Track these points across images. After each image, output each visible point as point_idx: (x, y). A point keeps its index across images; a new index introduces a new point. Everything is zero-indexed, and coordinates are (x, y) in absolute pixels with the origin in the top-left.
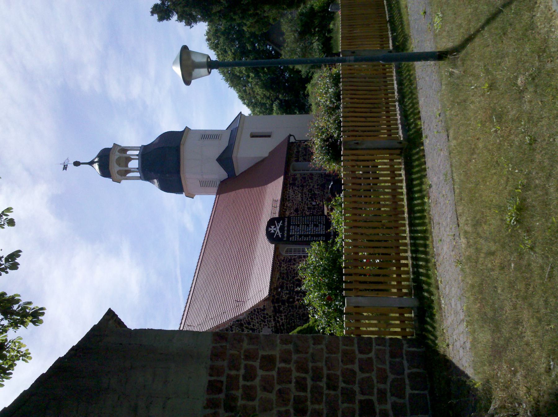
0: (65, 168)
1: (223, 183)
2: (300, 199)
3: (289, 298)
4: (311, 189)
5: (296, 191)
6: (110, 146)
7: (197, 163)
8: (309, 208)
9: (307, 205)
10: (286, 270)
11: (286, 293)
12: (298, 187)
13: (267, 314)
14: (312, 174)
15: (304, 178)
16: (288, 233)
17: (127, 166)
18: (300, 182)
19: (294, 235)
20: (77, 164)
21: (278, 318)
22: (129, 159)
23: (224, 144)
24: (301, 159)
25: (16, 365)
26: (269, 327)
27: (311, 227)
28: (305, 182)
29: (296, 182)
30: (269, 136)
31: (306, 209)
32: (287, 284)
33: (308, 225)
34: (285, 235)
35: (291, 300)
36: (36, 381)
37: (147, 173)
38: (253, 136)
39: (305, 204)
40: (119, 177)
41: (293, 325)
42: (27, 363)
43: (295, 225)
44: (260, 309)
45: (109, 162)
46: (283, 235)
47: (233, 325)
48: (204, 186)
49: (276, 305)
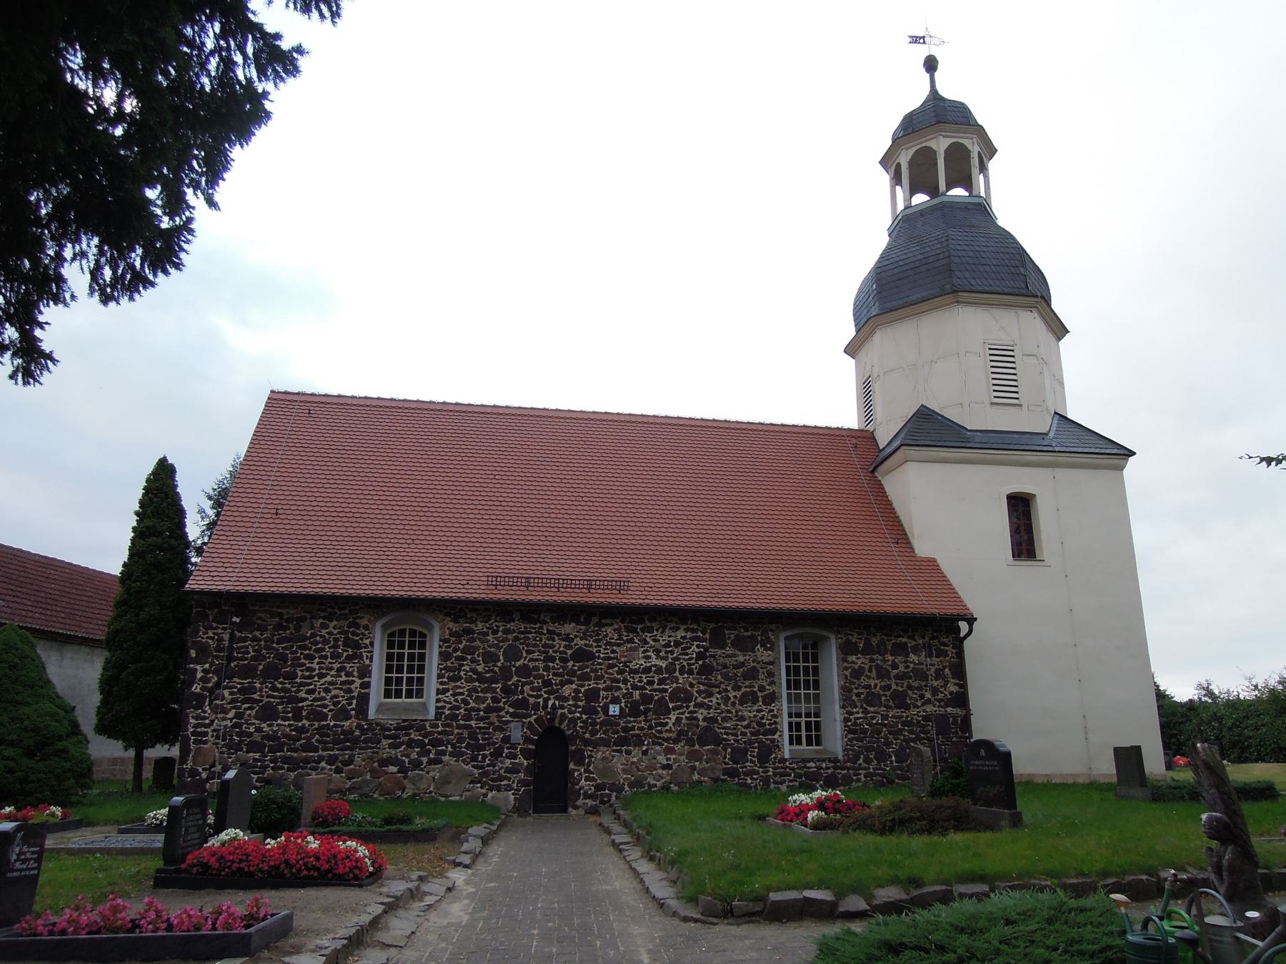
0: (916, 40)
5: (677, 652)
7: (951, 355)
11: (221, 640)
20: (931, 65)
32: (254, 639)
36: (94, 571)
42: (214, 212)
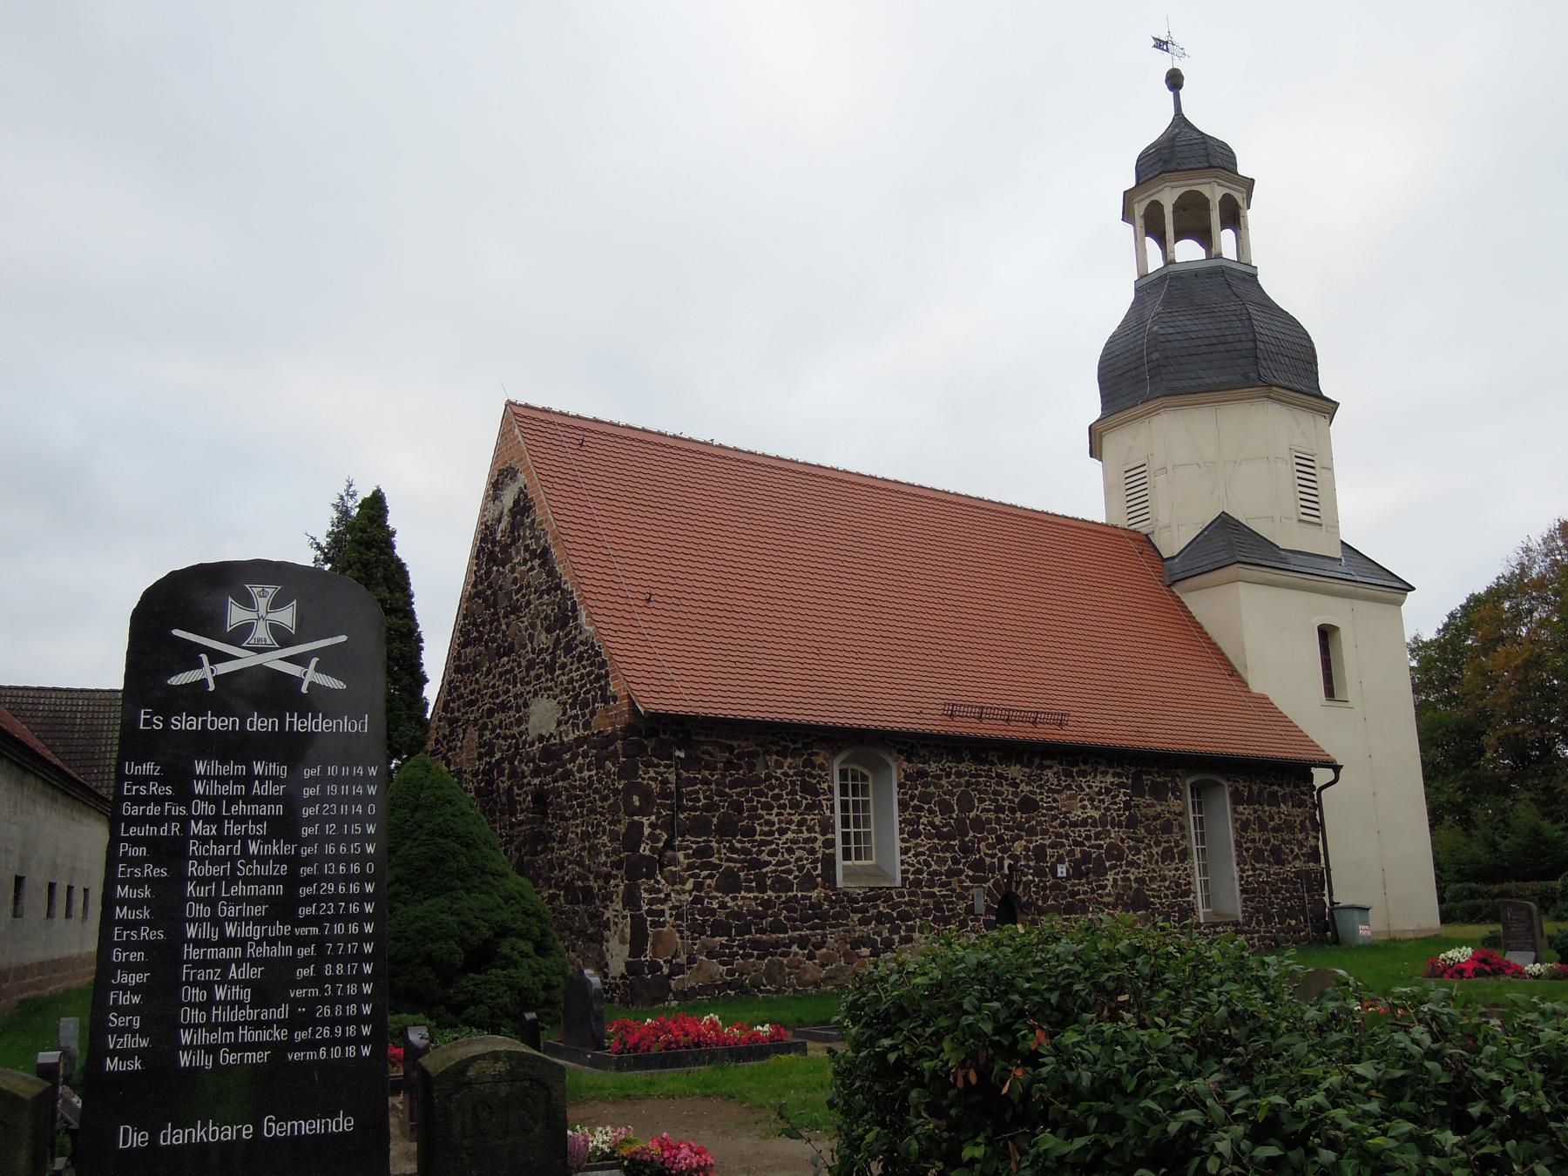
0: (1161, 44)
2: (1077, 814)
3: (646, 794)
5: (1108, 799)
6: (1243, 170)
7: (1210, 460)
8: (1040, 853)
9: (1052, 846)
10: (769, 777)
11: (665, 782)
12: (1127, 805)
13: (593, 713)
14: (1185, 855)
15: (1167, 829)
16: (208, 745)
17: (1179, 237)
18: (1150, 812)
19: (184, 796)
20: (1175, 81)
21: (585, 755)
22: (1205, 238)
23: (1289, 536)
24: (1246, 811)
26: (559, 724)
27: (263, 942)
28: (1149, 831)
29: (1148, 799)
30: (1330, 692)
31: (1038, 840)
32: (706, 782)
33: (282, 909)
34: (185, 723)
37: (1160, 293)
38: (1326, 634)
39: (1058, 835)
40: (1139, 210)
41: (568, 813)
43: (291, 802)
44: (608, 684)
45: (1187, 180)
46: (196, 698)
47: (563, 591)
48: (1133, 484)
49: (619, 744)
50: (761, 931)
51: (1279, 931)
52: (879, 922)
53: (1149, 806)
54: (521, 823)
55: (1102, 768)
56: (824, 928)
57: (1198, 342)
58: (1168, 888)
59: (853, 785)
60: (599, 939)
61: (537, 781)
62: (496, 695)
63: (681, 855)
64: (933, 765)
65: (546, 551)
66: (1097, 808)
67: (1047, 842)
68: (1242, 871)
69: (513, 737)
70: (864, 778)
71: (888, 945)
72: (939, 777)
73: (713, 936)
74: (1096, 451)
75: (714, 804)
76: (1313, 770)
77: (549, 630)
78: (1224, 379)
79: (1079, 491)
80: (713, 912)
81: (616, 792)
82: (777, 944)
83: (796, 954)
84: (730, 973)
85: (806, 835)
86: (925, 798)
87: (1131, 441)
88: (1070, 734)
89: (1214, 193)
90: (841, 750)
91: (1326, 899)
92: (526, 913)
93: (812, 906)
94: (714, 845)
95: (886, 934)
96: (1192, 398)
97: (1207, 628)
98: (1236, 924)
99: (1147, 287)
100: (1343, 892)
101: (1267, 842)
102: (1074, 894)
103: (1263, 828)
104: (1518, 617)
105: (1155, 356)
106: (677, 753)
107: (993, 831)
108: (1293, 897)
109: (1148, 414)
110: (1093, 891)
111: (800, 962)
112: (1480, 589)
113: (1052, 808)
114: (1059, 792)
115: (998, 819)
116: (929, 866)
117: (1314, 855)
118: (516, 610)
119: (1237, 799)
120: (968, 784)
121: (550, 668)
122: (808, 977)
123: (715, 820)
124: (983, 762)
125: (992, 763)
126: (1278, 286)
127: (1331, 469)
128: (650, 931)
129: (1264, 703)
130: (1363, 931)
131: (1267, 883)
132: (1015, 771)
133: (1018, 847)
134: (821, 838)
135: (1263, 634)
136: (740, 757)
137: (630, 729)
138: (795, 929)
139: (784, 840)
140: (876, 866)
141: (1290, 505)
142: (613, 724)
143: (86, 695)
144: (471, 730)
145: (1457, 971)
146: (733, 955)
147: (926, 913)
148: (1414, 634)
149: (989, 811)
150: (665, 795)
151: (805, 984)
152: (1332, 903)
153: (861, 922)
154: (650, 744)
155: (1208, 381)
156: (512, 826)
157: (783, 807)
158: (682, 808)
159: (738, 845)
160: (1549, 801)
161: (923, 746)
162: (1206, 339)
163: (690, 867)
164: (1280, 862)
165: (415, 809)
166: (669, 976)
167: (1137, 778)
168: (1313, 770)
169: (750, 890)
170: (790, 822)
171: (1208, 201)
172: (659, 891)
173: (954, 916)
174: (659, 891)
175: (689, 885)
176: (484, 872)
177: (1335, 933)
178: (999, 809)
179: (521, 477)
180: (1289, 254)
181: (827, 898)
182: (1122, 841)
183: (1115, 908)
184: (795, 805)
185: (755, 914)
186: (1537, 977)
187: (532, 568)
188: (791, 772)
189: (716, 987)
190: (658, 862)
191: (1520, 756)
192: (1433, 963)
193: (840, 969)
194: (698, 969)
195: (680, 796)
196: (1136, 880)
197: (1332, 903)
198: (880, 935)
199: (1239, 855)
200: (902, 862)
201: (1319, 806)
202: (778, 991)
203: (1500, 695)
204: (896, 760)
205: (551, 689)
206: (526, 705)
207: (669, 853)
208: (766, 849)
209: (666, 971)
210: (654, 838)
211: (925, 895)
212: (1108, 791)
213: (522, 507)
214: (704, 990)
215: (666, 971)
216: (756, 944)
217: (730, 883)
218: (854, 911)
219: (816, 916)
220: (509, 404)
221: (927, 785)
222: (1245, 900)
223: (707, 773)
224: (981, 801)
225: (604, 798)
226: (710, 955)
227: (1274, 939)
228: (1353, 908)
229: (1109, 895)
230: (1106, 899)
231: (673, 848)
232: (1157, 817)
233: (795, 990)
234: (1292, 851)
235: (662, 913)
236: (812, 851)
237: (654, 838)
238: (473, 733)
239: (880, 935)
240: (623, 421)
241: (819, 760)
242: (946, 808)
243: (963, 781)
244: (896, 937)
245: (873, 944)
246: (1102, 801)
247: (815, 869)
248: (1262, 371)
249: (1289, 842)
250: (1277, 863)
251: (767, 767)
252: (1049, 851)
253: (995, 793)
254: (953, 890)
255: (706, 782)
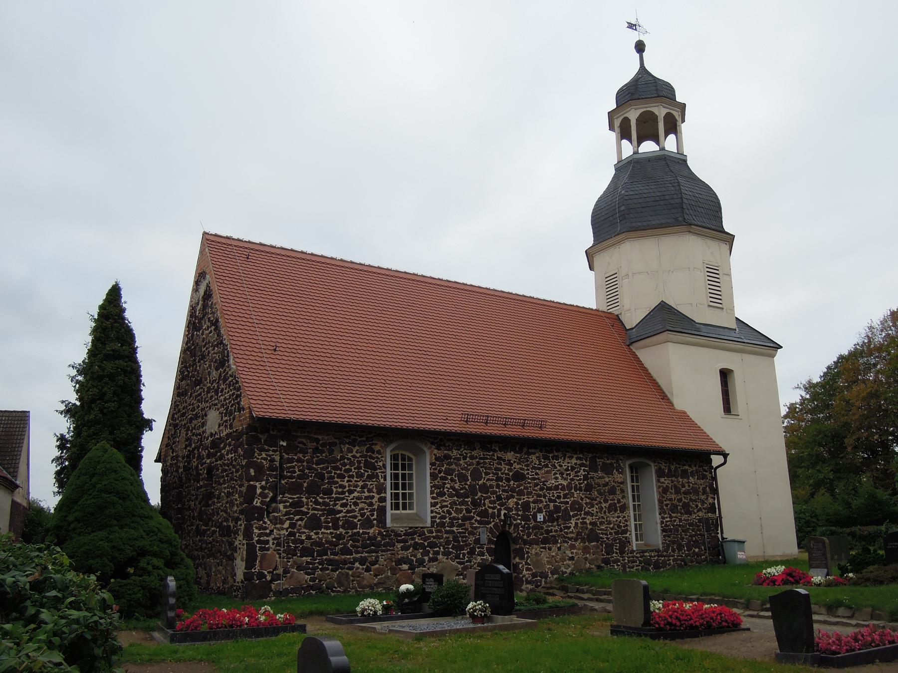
0: (631, 26)
1: (617, 320)
2: (552, 482)
3: (259, 469)
4: (580, 509)
6: (679, 99)
7: (661, 268)
8: (526, 506)
9: (534, 502)
10: (342, 458)
11: (273, 460)
12: (586, 478)
14: (624, 508)
15: (612, 491)
20: (640, 47)
23: (702, 315)
24: (666, 481)
25: (821, 377)
28: (600, 493)
29: (600, 474)
31: (525, 498)
32: (300, 461)
35: (252, 472)
38: (725, 375)
40: (617, 123)
45: (646, 106)
47: (224, 345)
48: (610, 285)
50: (336, 554)
51: (686, 556)
52: (415, 548)
53: (600, 478)
54: (201, 487)
55: (568, 454)
56: (377, 552)
57: (648, 199)
58: (612, 529)
59: (401, 464)
60: (232, 559)
61: (208, 461)
62: (193, 410)
63: (281, 506)
64: (455, 452)
65: (217, 321)
66: (566, 479)
67: (531, 500)
68: (663, 518)
69: (200, 434)
70: (410, 459)
71: (421, 563)
72: (459, 459)
73: (301, 556)
74: (591, 268)
75: (305, 474)
76: (712, 457)
77: (217, 369)
78: (663, 221)
79: (580, 289)
80: (302, 542)
81: (242, 467)
82: (345, 562)
83: (358, 568)
84: (313, 580)
85: (367, 494)
86: (449, 472)
87: (611, 259)
88: (548, 433)
89: (661, 112)
90: (391, 442)
91: (719, 535)
92: (161, 541)
93: (370, 538)
94: (304, 500)
95: (419, 556)
96: (643, 232)
97: (650, 371)
98: (658, 551)
99: (622, 167)
100: (730, 531)
101: (680, 500)
102: (548, 532)
103: (677, 492)
104: (869, 368)
105: (622, 208)
106: (282, 443)
107: (494, 493)
108: (697, 535)
109: (619, 242)
110: (561, 530)
111: (361, 573)
112: (845, 352)
113: (534, 479)
114: (540, 469)
115: (498, 486)
116: (450, 514)
117: (712, 509)
118: (203, 357)
119: (660, 474)
120: (478, 463)
121: (217, 392)
122: (365, 582)
123: (305, 485)
124: (489, 450)
125: (495, 451)
126: (699, 167)
127: (729, 275)
128: (259, 553)
129: (683, 416)
130: (741, 555)
131: (680, 526)
132: (510, 456)
133: (511, 503)
134: (377, 496)
135: (686, 376)
136: (323, 445)
137: (251, 427)
138: (357, 552)
139: (352, 497)
140: (416, 514)
141: (703, 296)
142: (242, 425)
143: (8, 414)
144: (183, 431)
145: (772, 581)
146: (315, 569)
147: (448, 542)
148: (808, 379)
149: (492, 480)
150: (271, 468)
151: (363, 587)
152: (723, 538)
153: (403, 548)
154: (263, 437)
155: (654, 223)
156: (198, 488)
157: (352, 476)
158: (282, 477)
159: (321, 500)
160: (885, 478)
161: (449, 440)
162: (657, 199)
163: (287, 513)
164: (689, 513)
165: (94, 475)
166: (271, 581)
167: (593, 460)
168: (712, 457)
169: (327, 528)
170: (357, 486)
171: (657, 117)
172: (266, 528)
173: (466, 545)
174: (266, 528)
175: (286, 525)
176: (134, 516)
177: (724, 557)
178: (500, 479)
179: (208, 276)
180: (705, 146)
181: (380, 533)
182: (582, 499)
183: (576, 540)
184: (360, 476)
185: (331, 543)
186: (819, 585)
187: (211, 332)
188: (358, 455)
189: (303, 588)
190: (268, 509)
191: (871, 449)
192: (759, 575)
193: (387, 578)
194: (291, 577)
195: (282, 469)
196: (591, 523)
197: (723, 538)
198: (415, 556)
199: (661, 508)
200: (432, 512)
201: (715, 479)
202: (344, 592)
203: (854, 414)
204: (430, 448)
205: (216, 405)
206: (206, 415)
207: (274, 505)
208: (340, 503)
209: (269, 578)
210: (263, 495)
211: (447, 532)
212: (573, 468)
213: (208, 295)
214: (293, 591)
215: (269, 578)
216: (330, 562)
217: (314, 524)
218: (399, 542)
219: (372, 544)
220: (205, 233)
221: (450, 464)
222: (664, 536)
223: (301, 456)
224: (486, 474)
225: (237, 471)
226: (299, 568)
227: (683, 560)
228: (734, 541)
229: (572, 532)
230: (570, 535)
231: (276, 502)
232: (606, 484)
233: (357, 591)
234: (697, 506)
235: (267, 542)
236: (371, 504)
237: (263, 495)
238: (183, 432)
239: (415, 556)
240: (339, 257)
241: (377, 448)
242: (462, 478)
243: (474, 461)
244: (426, 558)
245: (410, 562)
246: (569, 475)
247: (373, 515)
248: (686, 217)
249: (695, 501)
250: (686, 513)
251: (342, 452)
252: (532, 505)
253: (496, 469)
254: (467, 529)
255: (300, 461)
